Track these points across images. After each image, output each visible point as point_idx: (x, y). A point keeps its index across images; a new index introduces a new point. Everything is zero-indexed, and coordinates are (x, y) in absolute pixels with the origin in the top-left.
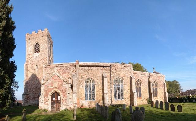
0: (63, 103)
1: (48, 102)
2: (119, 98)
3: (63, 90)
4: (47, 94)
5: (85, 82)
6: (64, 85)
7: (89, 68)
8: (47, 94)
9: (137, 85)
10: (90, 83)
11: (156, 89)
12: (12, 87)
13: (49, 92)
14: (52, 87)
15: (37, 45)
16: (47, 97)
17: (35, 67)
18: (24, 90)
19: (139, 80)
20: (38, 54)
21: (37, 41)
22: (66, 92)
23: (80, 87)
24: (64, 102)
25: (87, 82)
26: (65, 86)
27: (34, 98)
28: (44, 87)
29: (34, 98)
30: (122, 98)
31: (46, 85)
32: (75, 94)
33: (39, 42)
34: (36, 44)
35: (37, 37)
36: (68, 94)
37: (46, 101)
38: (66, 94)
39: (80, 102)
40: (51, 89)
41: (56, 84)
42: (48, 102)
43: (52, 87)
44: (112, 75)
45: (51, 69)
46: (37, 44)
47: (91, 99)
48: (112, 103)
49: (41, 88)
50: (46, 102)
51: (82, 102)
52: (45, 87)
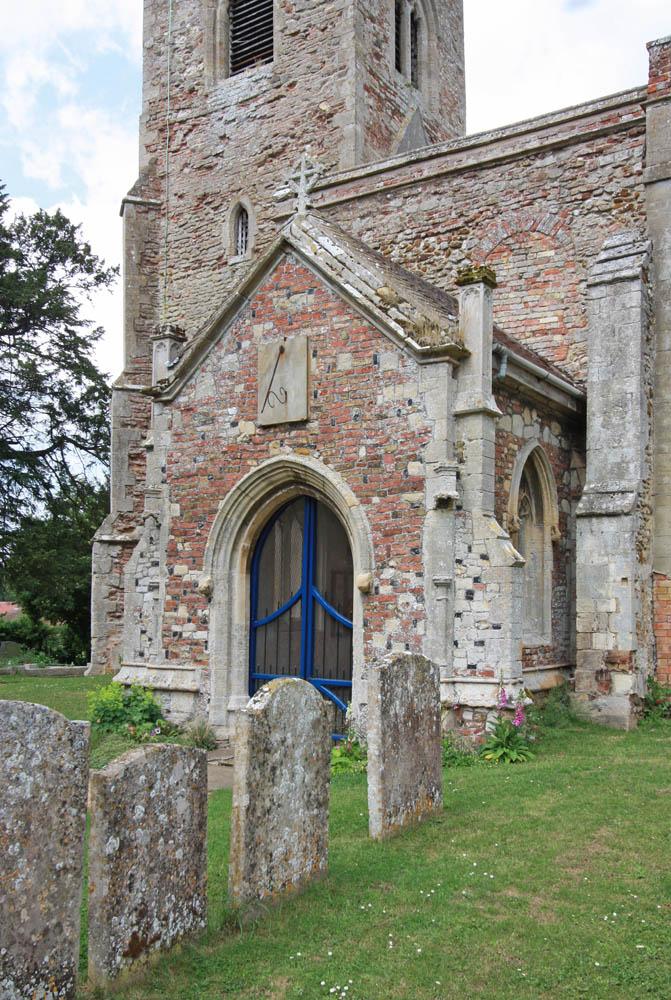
1: (204, 623)
3: (374, 462)
6: (396, 379)
17: (225, 230)
22: (418, 485)
24: (393, 625)
26: (408, 391)
28: (167, 439)
31: (188, 410)
32: (609, 526)
37: (183, 612)
40: (237, 454)
43: (248, 428)
50: (188, 630)
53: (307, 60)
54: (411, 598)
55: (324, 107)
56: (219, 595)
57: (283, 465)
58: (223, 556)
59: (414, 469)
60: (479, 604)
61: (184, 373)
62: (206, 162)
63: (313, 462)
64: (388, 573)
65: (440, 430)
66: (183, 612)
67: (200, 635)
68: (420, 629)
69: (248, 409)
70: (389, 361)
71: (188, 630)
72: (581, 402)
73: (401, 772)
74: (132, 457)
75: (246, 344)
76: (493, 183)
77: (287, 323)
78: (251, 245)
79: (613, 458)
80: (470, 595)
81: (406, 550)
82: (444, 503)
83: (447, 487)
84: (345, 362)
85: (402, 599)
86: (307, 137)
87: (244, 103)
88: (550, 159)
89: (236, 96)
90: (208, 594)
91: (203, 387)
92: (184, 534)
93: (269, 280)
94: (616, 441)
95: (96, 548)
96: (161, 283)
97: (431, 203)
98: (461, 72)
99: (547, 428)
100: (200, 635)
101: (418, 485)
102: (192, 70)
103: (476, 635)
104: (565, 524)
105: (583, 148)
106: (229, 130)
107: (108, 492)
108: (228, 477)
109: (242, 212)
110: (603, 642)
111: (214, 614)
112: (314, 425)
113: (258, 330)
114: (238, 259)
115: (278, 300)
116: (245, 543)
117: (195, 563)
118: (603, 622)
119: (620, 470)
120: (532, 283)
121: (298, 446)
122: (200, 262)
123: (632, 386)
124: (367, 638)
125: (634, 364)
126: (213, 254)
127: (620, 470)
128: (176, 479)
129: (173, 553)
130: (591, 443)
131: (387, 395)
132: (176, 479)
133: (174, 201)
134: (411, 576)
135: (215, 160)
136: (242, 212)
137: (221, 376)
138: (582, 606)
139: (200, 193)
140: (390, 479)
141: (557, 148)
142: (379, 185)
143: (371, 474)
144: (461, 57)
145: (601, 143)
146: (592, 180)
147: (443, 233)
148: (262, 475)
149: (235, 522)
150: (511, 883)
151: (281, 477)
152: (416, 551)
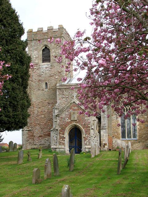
0: (86, 142)
1: (64, 141)
3: (85, 125)
4: (63, 130)
12: (77, 108)
15: (46, 50)
16: (64, 134)
17: (44, 86)
18: (14, 132)
20: (46, 65)
21: (45, 43)
22: (89, 127)
24: (87, 140)
27: (41, 136)
28: (59, 121)
29: (41, 136)
31: (61, 118)
32: (104, 130)
33: (49, 45)
34: (44, 48)
37: (61, 140)
38: (89, 130)
39: (114, 142)
40: (68, 123)
41: (76, 116)
45: (69, 91)
46: (46, 47)
47: (131, 137)
50: (62, 142)
51: (116, 142)
52: (60, 121)
54: (89, 138)
55: (59, 71)
57: (74, 124)
59: (89, 126)
60: (96, 138)
62: (40, 75)
63: (78, 124)
64: (86, 136)
66: (61, 140)
67: (64, 142)
68: (90, 141)
69: (70, 118)
71: (62, 142)
72: (100, 117)
73: (124, 125)
75: (69, 112)
78: (48, 88)
79: (104, 123)
80: (95, 138)
81: (88, 133)
85: (88, 138)
86: (57, 75)
87: (46, 68)
91: (63, 116)
92: (61, 131)
96: (32, 91)
100: (64, 142)
103: (95, 141)
108: (67, 125)
109: (46, 83)
110: (104, 142)
112: (78, 121)
114: (46, 90)
116: (69, 132)
118: (104, 140)
119: (105, 124)
121: (75, 123)
122: (39, 90)
124: (84, 142)
126: (42, 89)
127: (105, 124)
128: (60, 125)
130: (101, 121)
131: (86, 118)
133: (34, 80)
134: (89, 136)
135: (41, 75)
136: (46, 83)
137: (66, 115)
139: (39, 79)
140: (87, 127)
147: (29, 41)
149: (68, 130)
151: (74, 125)
152: (89, 133)
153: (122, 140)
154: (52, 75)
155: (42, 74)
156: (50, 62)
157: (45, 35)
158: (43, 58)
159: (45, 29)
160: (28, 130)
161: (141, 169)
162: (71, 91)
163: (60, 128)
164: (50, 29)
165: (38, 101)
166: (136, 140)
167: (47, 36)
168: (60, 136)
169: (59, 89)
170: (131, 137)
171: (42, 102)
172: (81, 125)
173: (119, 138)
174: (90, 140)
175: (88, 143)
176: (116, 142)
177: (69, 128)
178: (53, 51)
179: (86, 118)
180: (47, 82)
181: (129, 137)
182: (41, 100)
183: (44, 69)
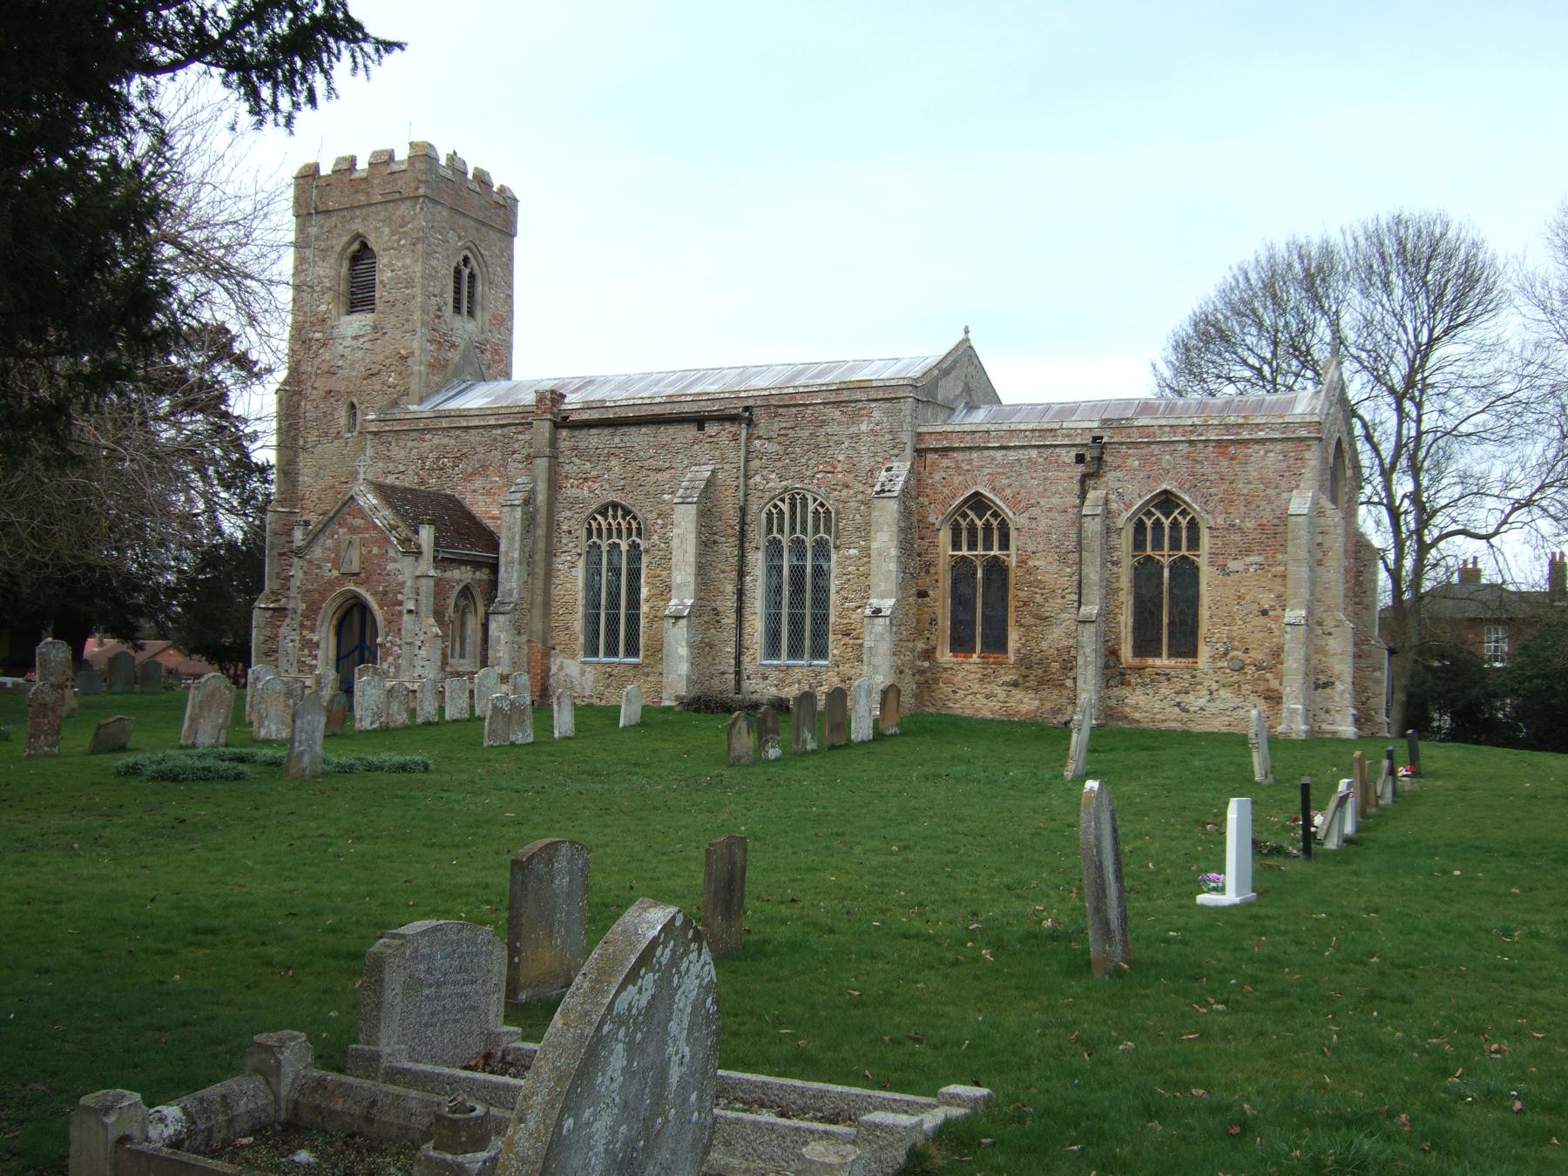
1: (315, 657)
2: (795, 651)
3: (385, 593)
4: (313, 610)
5: (590, 531)
6: (395, 560)
7: (618, 438)
8: (313, 610)
9: (988, 547)
10: (595, 539)
11: (1186, 573)
13: (324, 600)
14: (335, 573)
19: (977, 503)
20: (354, 325)
22: (401, 603)
23: (561, 563)
24: (391, 659)
25: (600, 535)
26: (397, 566)
28: (300, 574)
30: (820, 651)
31: (310, 561)
32: (501, 618)
34: (356, 246)
35: (363, 198)
36: (406, 617)
37: (306, 652)
39: (554, 669)
40: (332, 584)
41: (354, 561)
42: (315, 657)
43: (335, 573)
44: (758, 478)
45: (410, 444)
48: (745, 684)
49: (1362, 535)
53: (394, 321)
56: (323, 645)
58: (324, 628)
60: (423, 652)
61: (309, 545)
63: (362, 591)
65: (409, 583)
66: (306, 652)
69: (337, 565)
70: (392, 553)
71: (309, 660)
74: (281, 554)
76: (474, 437)
77: (353, 530)
82: (410, 612)
83: (411, 605)
84: (375, 550)
87: (356, 338)
88: (499, 431)
89: (350, 332)
90: (317, 645)
91: (317, 553)
92: (307, 617)
93: (346, 510)
94: (509, 580)
95: (256, 613)
97: (445, 441)
98: (510, 297)
99: (1437, 234)
101: (401, 603)
102: (323, 307)
104: (487, 615)
105: (513, 429)
106: (347, 352)
107: (262, 550)
111: (320, 653)
113: (341, 531)
115: (350, 520)
117: (312, 630)
119: (511, 591)
120: (488, 493)
123: (516, 555)
125: (517, 545)
127: (511, 591)
128: (306, 593)
129: (302, 626)
131: (391, 566)
132: (306, 593)
136: (353, 406)
138: (491, 653)
140: (390, 600)
141: (502, 426)
142: (421, 426)
143: (383, 597)
144: (511, 287)
145: (520, 428)
146: (516, 446)
148: (342, 594)
149: (330, 613)
150: (856, 1074)
153: (585, 663)
154: (376, 368)
155: (340, 363)
156: (373, 311)
157: (357, 191)
158: (353, 294)
159: (326, 170)
160: (273, 609)
161: (1390, 847)
162: (415, 444)
163: (304, 606)
164: (383, 160)
165: (322, 484)
166: (636, 666)
167: (368, 194)
168: (303, 638)
169: (376, 434)
170: (596, 654)
171: (332, 487)
172: (375, 594)
173: (573, 656)
174: (399, 656)
175: (392, 669)
176: (561, 668)
177: (335, 605)
178: (385, 261)
179: (391, 566)
180: (355, 401)
181: (612, 650)
182: (331, 481)
183: (348, 342)
